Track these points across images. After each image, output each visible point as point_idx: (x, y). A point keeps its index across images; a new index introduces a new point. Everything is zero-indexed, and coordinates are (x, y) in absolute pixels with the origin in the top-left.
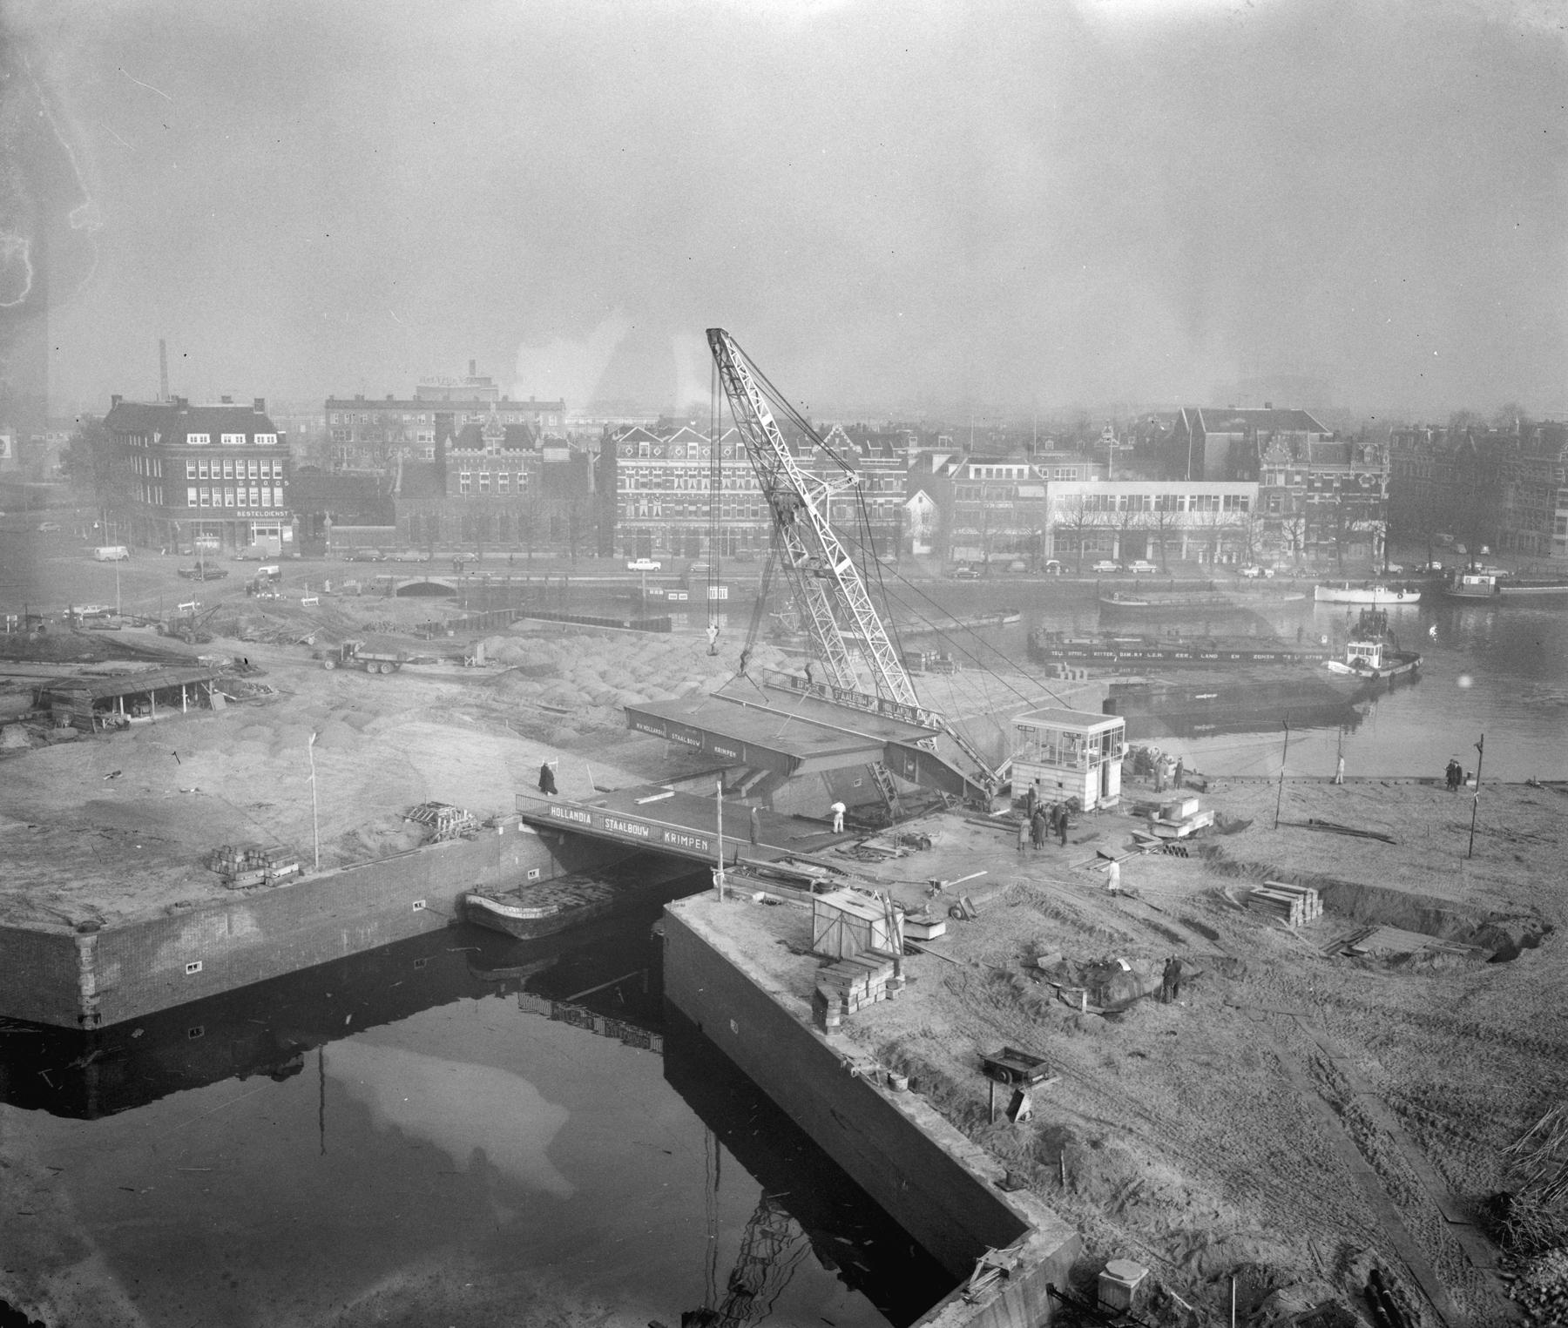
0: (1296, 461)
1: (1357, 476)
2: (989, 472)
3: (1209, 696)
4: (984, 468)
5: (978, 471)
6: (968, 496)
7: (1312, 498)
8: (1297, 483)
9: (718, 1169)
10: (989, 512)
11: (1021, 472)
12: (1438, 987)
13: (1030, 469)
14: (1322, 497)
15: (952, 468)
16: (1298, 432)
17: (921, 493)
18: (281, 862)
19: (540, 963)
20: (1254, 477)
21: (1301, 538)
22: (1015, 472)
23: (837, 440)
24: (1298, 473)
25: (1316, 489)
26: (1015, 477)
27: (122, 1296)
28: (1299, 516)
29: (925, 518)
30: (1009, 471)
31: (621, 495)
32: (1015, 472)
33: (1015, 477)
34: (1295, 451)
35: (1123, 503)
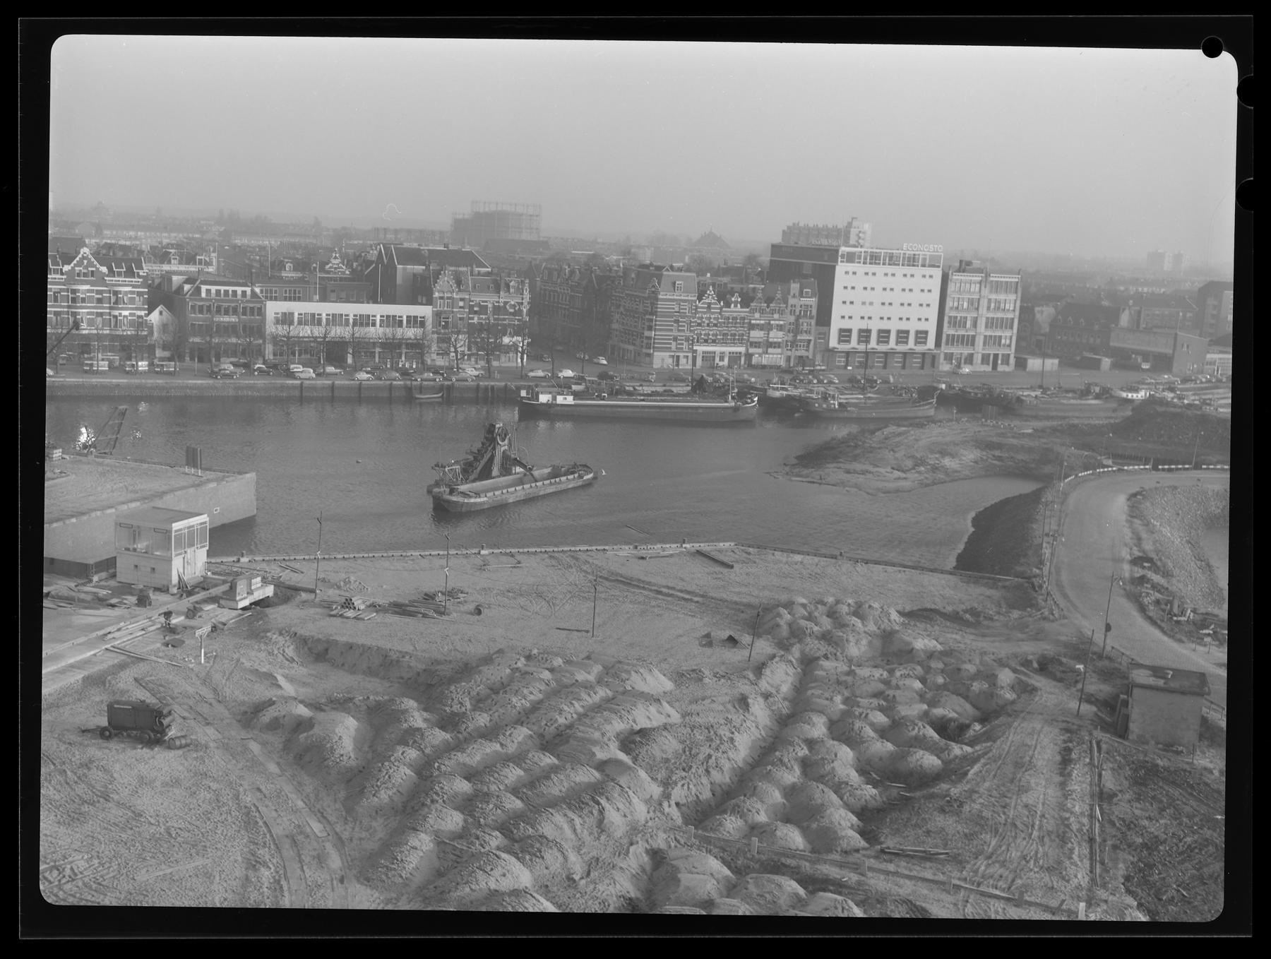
0: (460, 291)
1: (506, 303)
2: (208, 291)
7: (473, 319)
8: (461, 307)
11: (244, 293)
14: (479, 319)
15: (187, 287)
20: (429, 302)
22: (239, 293)
23: (85, 262)
24: (462, 300)
25: (476, 312)
26: (239, 297)
30: (235, 292)
32: (239, 293)
33: (239, 297)
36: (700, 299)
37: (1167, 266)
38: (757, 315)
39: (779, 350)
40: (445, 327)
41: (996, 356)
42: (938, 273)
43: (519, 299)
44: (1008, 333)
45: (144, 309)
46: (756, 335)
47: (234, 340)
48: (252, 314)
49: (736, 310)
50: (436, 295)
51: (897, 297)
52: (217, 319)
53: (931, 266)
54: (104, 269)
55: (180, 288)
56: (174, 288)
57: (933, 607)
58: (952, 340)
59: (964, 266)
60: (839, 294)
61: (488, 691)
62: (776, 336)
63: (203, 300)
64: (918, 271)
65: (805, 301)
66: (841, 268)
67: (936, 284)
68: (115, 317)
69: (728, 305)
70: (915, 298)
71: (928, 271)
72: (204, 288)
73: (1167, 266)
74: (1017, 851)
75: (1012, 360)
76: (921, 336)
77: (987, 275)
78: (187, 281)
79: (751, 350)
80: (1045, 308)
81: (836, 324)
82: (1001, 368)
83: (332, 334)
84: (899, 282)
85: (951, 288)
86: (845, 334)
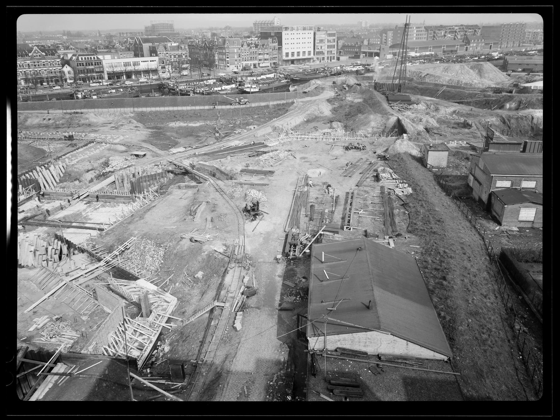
1: (181, 53)
2: (88, 58)
3: (202, 108)
4: (83, 57)
5: (82, 59)
6: (89, 65)
9: (94, 224)
10: (87, 70)
12: (298, 156)
13: (97, 57)
15: (74, 58)
16: (166, 43)
17: (66, 65)
18: (515, 233)
19: (488, 225)
20: (157, 55)
21: (171, 70)
26: (93, 59)
27: (480, 375)
28: (169, 65)
29: (69, 73)
30: (88, 58)
31: (188, 64)
34: (165, 48)
35: (124, 64)
36: (242, 46)
37: (363, 25)
38: (260, 50)
39: (268, 61)
40: (163, 63)
41: (331, 57)
42: (312, 32)
43: (184, 53)
44: (334, 49)
45: (61, 66)
46: (261, 57)
47: (83, 75)
48: (80, 65)
49: (254, 49)
50: (159, 53)
51: (295, 41)
52: (88, 67)
53: (310, 30)
54: (44, 54)
55: (71, 58)
56: (69, 58)
57: (259, 142)
58: (318, 53)
59: (319, 30)
60: (284, 42)
61: (529, 128)
62: (266, 57)
63: (80, 61)
64: (307, 32)
65: (274, 44)
66: (284, 33)
67: (312, 36)
68: (36, 71)
69: (251, 48)
70: (290, 41)
71: (310, 32)
72: (80, 58)
73: (363, 25)
74: (175, 241)
75: (336, 58)
76: (309, 53)
77: (327, 31)
78: (73, 55)
79: (260, 62)
80: (341, 41)
81: (284, 51)
82: (332, 61)
83: (128, 69)
84: (301, 36)
85: (317, 36)
86: (287, 54)
